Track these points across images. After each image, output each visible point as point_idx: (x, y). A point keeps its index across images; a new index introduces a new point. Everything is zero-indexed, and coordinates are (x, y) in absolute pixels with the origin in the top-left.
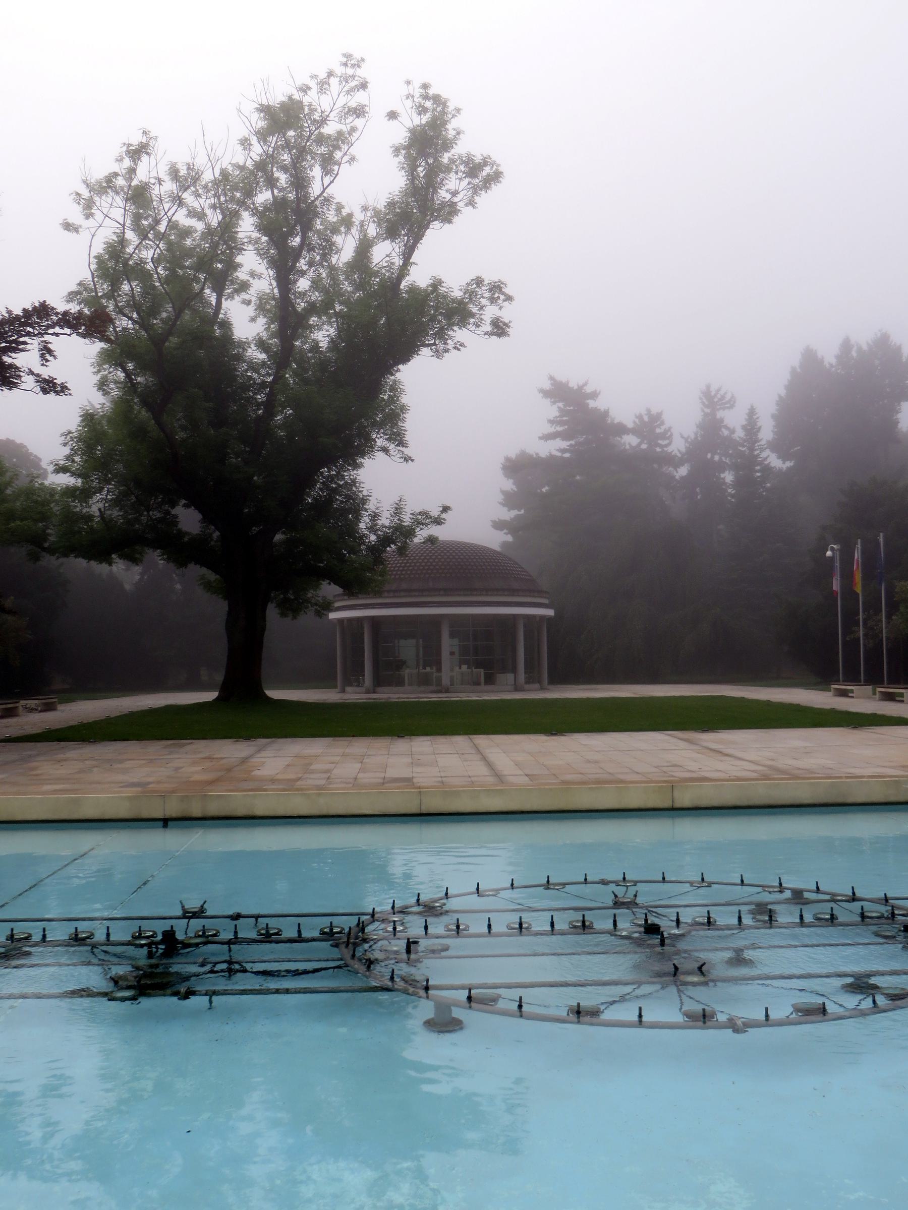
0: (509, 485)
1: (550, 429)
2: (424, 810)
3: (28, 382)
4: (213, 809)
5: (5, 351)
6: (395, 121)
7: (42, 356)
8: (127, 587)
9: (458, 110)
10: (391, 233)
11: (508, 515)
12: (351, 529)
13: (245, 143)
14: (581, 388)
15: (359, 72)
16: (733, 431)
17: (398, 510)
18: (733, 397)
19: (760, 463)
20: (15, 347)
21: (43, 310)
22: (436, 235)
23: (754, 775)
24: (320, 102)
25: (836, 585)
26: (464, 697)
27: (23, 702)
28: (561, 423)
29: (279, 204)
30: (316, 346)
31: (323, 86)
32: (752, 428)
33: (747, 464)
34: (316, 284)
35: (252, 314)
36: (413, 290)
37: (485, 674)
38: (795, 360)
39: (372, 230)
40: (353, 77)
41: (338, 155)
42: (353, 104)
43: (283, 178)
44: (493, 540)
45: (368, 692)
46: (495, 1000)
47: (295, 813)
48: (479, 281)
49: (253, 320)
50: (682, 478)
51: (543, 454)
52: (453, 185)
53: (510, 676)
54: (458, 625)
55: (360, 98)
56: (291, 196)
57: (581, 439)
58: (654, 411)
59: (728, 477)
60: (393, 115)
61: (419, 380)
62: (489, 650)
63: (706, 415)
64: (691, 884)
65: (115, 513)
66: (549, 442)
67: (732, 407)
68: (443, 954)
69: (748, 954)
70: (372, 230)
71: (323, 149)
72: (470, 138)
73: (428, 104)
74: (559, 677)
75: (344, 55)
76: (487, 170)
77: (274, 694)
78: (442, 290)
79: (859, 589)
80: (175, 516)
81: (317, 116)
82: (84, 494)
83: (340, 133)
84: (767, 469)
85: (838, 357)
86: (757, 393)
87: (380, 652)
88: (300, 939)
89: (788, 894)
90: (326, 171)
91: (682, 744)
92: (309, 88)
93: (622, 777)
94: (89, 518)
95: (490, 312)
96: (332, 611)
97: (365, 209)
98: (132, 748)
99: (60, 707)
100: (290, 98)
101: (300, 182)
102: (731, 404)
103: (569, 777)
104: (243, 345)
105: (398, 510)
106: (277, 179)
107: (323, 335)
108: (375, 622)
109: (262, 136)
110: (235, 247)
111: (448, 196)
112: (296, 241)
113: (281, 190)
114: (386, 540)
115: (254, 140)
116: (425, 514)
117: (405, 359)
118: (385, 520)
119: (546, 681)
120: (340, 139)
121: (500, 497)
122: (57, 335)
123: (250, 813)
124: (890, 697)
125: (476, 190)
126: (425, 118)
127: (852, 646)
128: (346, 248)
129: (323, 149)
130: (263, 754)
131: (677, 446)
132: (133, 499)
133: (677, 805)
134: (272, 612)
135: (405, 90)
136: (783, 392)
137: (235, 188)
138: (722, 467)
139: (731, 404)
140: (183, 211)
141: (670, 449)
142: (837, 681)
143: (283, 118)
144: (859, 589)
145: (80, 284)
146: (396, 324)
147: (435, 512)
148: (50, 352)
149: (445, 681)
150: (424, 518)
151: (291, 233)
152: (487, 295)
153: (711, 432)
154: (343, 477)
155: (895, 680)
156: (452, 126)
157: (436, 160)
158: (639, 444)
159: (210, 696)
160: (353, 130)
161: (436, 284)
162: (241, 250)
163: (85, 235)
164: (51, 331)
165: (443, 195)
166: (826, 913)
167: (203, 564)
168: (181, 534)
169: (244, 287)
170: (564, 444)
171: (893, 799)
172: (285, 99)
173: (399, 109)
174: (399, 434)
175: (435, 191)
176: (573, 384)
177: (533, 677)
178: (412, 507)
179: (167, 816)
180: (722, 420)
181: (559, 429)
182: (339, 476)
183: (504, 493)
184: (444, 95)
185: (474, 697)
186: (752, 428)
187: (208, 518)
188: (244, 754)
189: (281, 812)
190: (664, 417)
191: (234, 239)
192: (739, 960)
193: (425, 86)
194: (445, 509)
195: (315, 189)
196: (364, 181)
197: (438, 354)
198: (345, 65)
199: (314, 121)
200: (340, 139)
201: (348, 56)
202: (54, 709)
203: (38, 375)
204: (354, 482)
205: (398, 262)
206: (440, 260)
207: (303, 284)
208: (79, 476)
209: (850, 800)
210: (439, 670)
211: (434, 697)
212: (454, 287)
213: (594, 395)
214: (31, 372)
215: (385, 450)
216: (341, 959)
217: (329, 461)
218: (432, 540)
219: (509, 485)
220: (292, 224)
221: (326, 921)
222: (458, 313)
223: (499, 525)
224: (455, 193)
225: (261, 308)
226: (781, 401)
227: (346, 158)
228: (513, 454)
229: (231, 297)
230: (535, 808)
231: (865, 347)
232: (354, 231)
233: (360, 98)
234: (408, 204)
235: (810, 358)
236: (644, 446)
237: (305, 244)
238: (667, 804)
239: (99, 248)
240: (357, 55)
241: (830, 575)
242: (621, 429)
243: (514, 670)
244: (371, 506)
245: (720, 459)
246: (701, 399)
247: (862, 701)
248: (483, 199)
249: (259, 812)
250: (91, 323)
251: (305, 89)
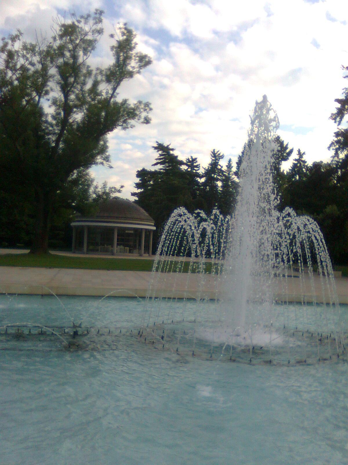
1: (155, 162)
6: (113, 39)
10: (108, 81)
12: (86, 191)
13: (54, 39)
18: (223, 155)
22: (125, 83)
24: (86, 27)
29: (66, 64)
36: (116, 103)
37: (129, 249)
39: (99, 78)
43: (68, 54)
50: (203, 183)
52: (133, 64)
60: (112, 36)
61: (114, 138)
66: (155, 166)
90: (85, 54)
95: (144, 114)
96: (74, 222)
101: (75, 57)
113: (68, 59)
119: (143, 251)
126: (125, 37)
137: (49, 55)
141: (198, 172)
146: (108, 116)
147: (118, 187)
151: (70, 76)
158: (188, 169)
161: (125, 101)
165: (129, 68)
175: (126, 66)
195: (80, 60)
196: (101, 59)
206: (128, 93)
207: (72, 97)
210: (112, 247)
212: (132, 102)
215: (102, 163)
220: (71, 72)
222: (132, 114)
236: (189, 170)
242: (181, 163)
244: (95, 183)
245: (217, 177)
246: (211, 154)
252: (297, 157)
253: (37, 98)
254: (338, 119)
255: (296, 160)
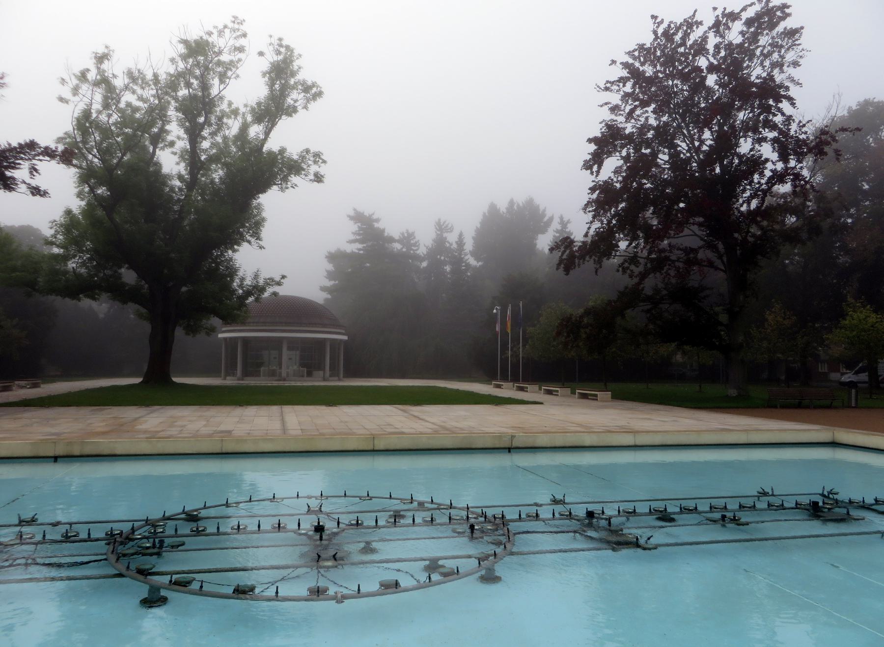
0: (330, 267)
2: (224, 451)
3: (23, 188)
4: (88, 450)
5: (7, 168)
7: (31, 173)
8: (101, 316)
9: (300, 55)
10: (258, 119)
11: (329, 283)
13: (172, 60)
14: (370, 216)
15: (241, 27)
16: (451, 244)
17: (256, 276)
19: (465, 262)
20: (14, 166)
21: (32, 145)
22: (284, 124)
23: (430, 431)
25: (498, 329)
26: (293, 384)
27: (16, 382)
28: (359, 234)
29: (192, 98)
30: (212, 182)
31: (221, 33)
32: (461, 243)
33: (457, 261)
34: (214, 145)
35: (178, 160)
36: (270, 153)
38: (485, 209)
40: (238, 30)
41: (229, 73)
42: (237, 45)
43: (195, 82)
44: (318, 296)
45: (239, 380)
46: (189, 583)
47: (142, 453)
48: (307, 151)
49: (178, 164)
51: (349, 250)
52: (295, 97)
53: (321, 373)
54: (293, 344)
55: (242, 42)
56: (200, 94)
57: (370, 244)
58: (410, 231)
59: (448, 268)
60: (261, 54)
61: (271, 202)
62: (311, 357)
63: (438, 235)
64: (360, 498)
65: (83, 270)
67: (451, 231)
68: (180, 548)
69: (374, 545)
70: (249, 118)
71: (220, 69)
72: (307, 70)
73: (283, 50)
74: (351, 373)
75: (234, 17)
76: (314, 90)
77: (174, 379)
78: (286, 154)
79: (509, 331)
80: (120, 274)
81: (216, 50)
82: (65, 258)
83: (232, 61)
84: (468, 265)
85: (507, 209)
86: (466, 227)
87: (252, 357)
88: (89, 539)
89: (415, 504)
90: (222, 82)
91: (400, 412)
92: (212, 33)
93: (404, 430)
94: (66, 272)
95: (314, 168)
97: (246, 106)
98: (72, 411)
99: (42, 386)
100: (201, 38)
101: (205, 86)
102: (451, 230)
103: (324, 431)
104: (169, 177)
105: (256, 276)
106: (192, 84)
107: (218, 174)
108: (246, 340)
109: (184, 58)
110: (165, 120)
111: (292, 102)
112: (202, 120)
114: (248, 293)
115: (178, 59)
116: (272, 279)
117: (263, 191)
118: (248, 282)
119: (342, 376)
120: (231, 65)
121: (325, 274)
122: (41, 160)
123: (113, 453)
124: (521, 389)
125: (308, 100)
126: (281, 57)
127: (505, 361)
128: (233, 127)
129: (220, 69)
130: (151, 415)
131: (422, 251)
132: (95, 263)
133: (376, 448)
134: (179, 332)
135: (269, 41)
136: (479, 226)
138: (445, 263)
139: (451, 230)
140: (135, 97)
141: (418, 252)
142: (496, 379)
143: (197, 49)
144: (509, 331)
145: (66, 133)
146: (259, 171)
147: (277, 279)
148: (36, 170)
149: (284, 374)
150: (271, 282)
151: (199, 115)
152: (312, 159)
153: (440, 243)
154: (225, 256)
155: (525, 380)
156: (295, 65)
157: (286, 81)
159: (137, 380)
160: (240, 60)
161: (282, 151)
162: (169, 122)
163: (71, 106)
164: (37, 158)
165: (289, 101)
166: (437, 515)
167: (136, 302)
168: (124, 285)
169: (172, 144)
170: (360, 246)
171: (497, 446)
172: (198, 38)
173: (265, 50)
174: (257, 233)
176: (366, 214)
177: (334, 373)
178: (264, 275)
179: (57, 454)
180: (446, 238)
181: (358, 237)
182: (222, 254)
183: (327, 271)
184: (292, 46)
185: (299, 384)
186: (461, 243)
187: (141, 276)
188: (137, 416)
189: (132, 452)
190: (416, 235)
191: (165, 116)
192: (368, 549)
193: (280, 39)
194: (283, 277)
195: (214, 91)
196: (244, 90)
197: (282, 190)
198: (234, 22)
199: (214, 52)
200: (231, 65)
201: (236, 17)
202: (39, 387)
203: (29, 184)
204: (231, 259)
205: (262, 137)
206: (285, 137)
207: (205, 144)
208: (62, 248)
209: (474, 446)
210: (281, 368)
211: (275, 383)
212: (294, 152)
213: (378, 220)
214: (24, 182)
215: (249, 242)
216: (105, 554)
217: (217, 246)
218: (275, 294)
219: (330, 267)
220: (199, 110)
221: (108, 527)
222: (295, 167)
223: (323, 289)
224: (296, 101)
225: (182, 157)
226: (478, 231)
227: (234, 76)
228: (333, 249)
229: (162, 149)
230: (292, 450)
231: (521, 205)
232: (240, 118)
233: (242, 42)
234: (269, 104)
235: (493, 208)
236: (404, 250)
237: (207, 122)
238: (370, 447)
239: (77, 113)
240: (241, 18)
241: (495, 323)
242: (391, 240)
243: (324, 370)
244: (240, 274)
247: (507, 391)
248: (312, 105)
249: (118, 452)
250: (67, 157)
251: (210, 34)
252: (559, 227)
253: (151, 149)
254: (595, 168)
255: (557, 231)
